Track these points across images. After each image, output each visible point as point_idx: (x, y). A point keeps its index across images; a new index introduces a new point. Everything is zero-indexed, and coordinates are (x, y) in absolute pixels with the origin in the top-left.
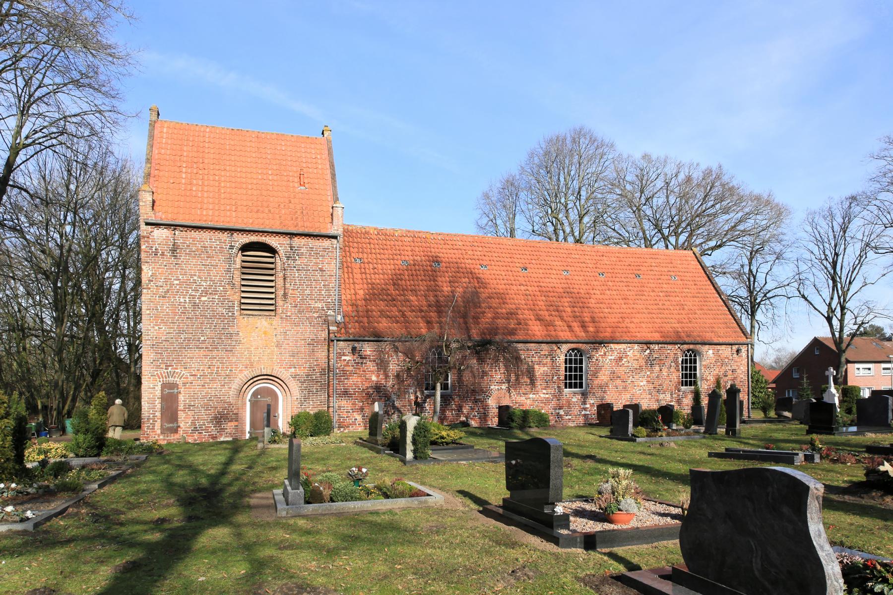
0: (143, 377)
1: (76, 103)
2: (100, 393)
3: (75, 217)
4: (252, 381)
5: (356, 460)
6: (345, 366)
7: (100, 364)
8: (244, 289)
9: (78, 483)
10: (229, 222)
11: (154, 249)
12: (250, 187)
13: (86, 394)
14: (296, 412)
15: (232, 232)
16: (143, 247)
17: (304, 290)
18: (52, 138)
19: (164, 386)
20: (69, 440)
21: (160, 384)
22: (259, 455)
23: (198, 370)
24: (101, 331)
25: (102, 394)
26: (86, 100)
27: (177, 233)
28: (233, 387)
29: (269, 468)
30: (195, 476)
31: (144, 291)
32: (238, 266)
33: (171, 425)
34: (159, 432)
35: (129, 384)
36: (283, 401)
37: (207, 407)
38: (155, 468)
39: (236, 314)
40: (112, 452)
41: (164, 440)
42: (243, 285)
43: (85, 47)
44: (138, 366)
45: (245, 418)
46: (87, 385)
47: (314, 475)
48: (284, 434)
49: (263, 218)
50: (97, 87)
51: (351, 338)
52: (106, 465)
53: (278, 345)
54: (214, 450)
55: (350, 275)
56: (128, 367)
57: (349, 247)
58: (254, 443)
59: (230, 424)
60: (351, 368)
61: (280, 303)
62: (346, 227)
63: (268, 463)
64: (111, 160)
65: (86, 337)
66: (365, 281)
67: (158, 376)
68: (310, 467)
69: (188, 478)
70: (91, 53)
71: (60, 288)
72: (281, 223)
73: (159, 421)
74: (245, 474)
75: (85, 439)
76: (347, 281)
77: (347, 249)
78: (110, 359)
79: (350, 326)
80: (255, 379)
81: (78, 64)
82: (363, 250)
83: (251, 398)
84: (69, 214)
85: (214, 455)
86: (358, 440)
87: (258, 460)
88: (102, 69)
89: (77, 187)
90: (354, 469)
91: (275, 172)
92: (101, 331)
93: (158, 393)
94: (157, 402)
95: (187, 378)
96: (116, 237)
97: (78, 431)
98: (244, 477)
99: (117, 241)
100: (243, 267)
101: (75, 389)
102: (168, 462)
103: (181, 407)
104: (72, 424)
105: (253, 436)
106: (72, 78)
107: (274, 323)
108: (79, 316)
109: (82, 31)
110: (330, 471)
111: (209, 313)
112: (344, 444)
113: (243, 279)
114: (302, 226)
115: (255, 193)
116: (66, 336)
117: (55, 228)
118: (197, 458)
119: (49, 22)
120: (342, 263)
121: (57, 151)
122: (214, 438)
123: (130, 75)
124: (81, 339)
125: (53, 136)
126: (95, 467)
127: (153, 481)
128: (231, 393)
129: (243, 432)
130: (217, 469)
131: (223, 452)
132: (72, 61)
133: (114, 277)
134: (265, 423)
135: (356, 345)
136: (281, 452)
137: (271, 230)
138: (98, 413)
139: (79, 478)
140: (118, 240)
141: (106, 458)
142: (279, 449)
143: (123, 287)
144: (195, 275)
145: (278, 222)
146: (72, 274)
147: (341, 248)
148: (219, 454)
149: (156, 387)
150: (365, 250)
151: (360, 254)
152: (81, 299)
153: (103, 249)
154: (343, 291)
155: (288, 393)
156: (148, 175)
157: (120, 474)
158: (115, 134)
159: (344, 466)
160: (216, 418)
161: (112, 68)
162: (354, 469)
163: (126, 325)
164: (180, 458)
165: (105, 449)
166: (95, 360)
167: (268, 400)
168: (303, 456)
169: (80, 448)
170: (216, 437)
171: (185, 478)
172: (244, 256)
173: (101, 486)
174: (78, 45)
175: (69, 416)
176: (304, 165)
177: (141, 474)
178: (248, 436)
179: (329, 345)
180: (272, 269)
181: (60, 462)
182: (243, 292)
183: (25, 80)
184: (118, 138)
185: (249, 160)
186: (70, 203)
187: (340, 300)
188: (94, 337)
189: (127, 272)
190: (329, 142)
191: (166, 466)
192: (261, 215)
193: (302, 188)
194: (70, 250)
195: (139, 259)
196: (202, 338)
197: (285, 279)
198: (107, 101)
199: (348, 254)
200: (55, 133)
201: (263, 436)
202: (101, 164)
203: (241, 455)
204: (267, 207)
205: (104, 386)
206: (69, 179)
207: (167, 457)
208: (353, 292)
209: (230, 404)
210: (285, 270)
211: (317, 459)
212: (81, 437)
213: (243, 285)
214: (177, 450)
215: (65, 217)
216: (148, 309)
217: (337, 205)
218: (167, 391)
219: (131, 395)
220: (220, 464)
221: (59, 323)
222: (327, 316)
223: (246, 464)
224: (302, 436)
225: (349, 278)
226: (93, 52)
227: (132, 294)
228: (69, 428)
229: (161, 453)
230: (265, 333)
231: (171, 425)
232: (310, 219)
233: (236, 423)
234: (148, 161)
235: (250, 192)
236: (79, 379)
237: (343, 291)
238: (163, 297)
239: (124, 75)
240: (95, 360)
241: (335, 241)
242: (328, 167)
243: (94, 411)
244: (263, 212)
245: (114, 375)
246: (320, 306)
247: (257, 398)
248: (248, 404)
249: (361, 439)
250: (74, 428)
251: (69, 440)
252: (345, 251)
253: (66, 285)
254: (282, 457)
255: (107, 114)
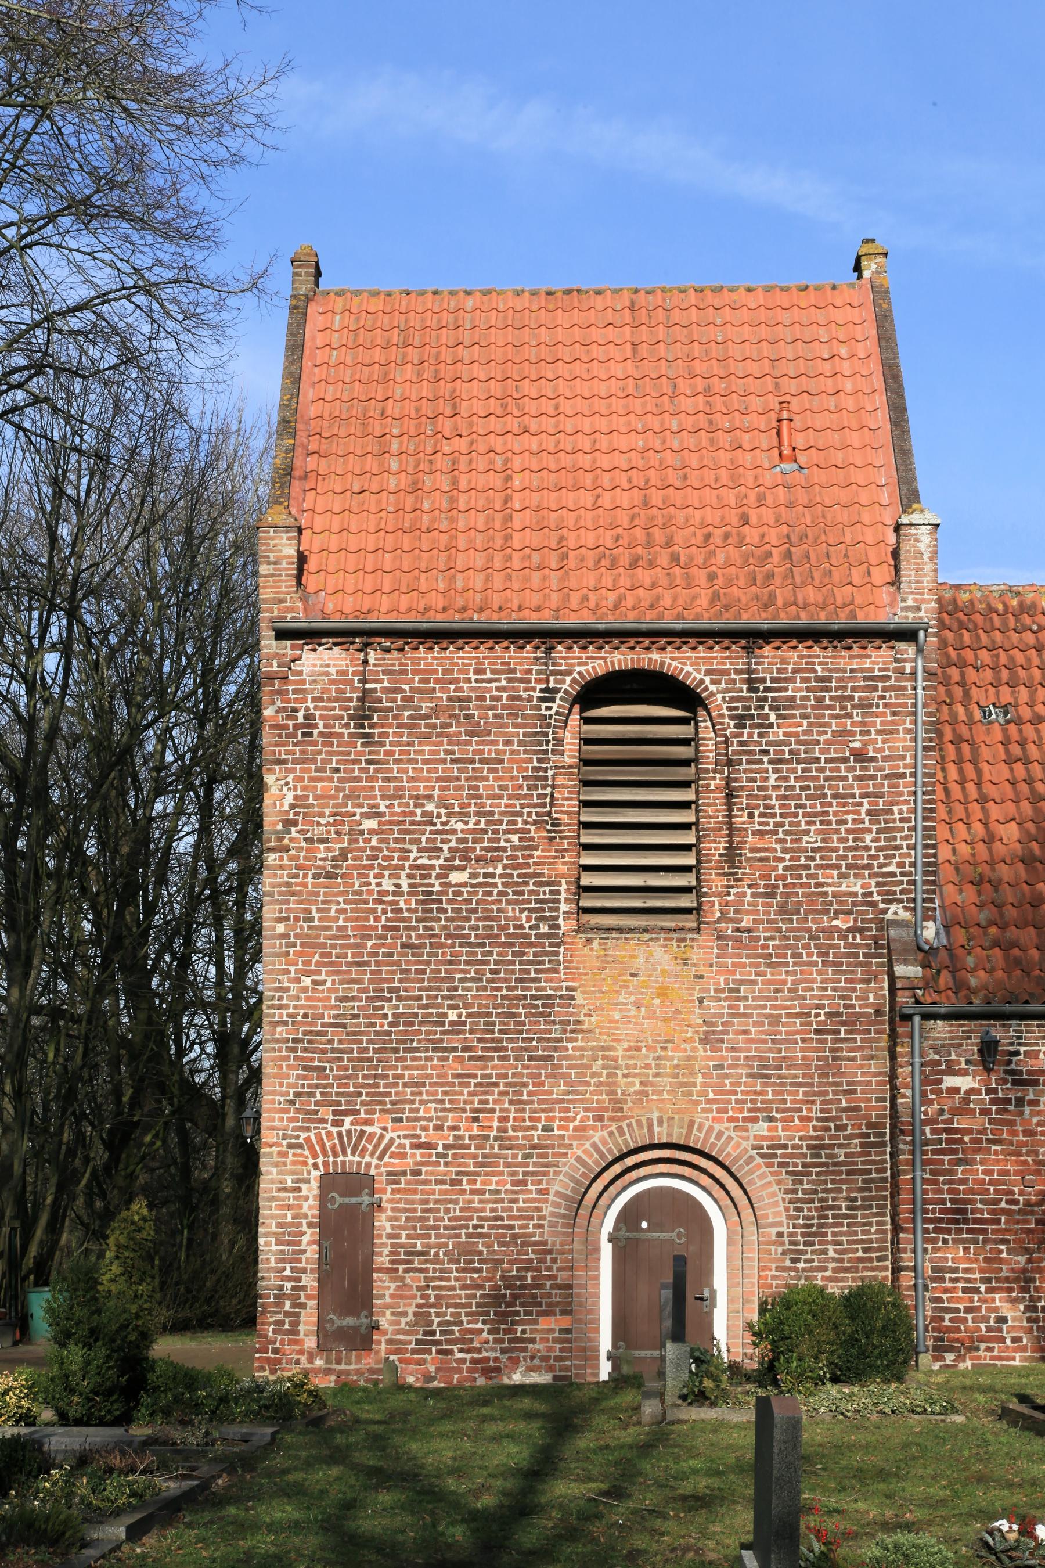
0: (264, 1150)
1: (80, 270)
2: (135, 1207)
3: (70, 626)
4: (617, 1168)
5: (1010, 1485)
6: (955, 1111)
7: (135, 1103)
8: (587, 838)
9: (69, 1517)
10: (538, 609)
11: (301, 715)
12: (606, 480)
13: (89, 1204)
14: (777, 1283)
15: (550, 642)
16: (268, 712)
17: (798, 834)
18: (11, 387)
19: (330, 1182)
20: (37, 1362)
21: (316, 1174)
22: (645, 1448)
23: (438, 1128)
24: (138, 993)
25: (139, 1208)
26: (107, 256)
27: (372, 657)
28: (556, 1187)
29: (684, 1498)
30: (432, 1513)
31: (271, 858)
32: (570, 757)
33: (350, 1321)
34: (311, 1343)
35: (217, 1173)
36: (730, 1242)
37: (465, 1256)
38: (299, 1476)
39: (565, 925)
40: (167, 1413)
41: (328, 1372)
42: (588, 825)
43: (108, 98)
44: (248, 1113)
45: (597, 1304)
46: (94, 1173)
47: (850, 1536)
48: (734, 1368)
49: (654, 586)
50: (138, 211)
51: (977, 1004)
52: (150, 1459)
53: (710, 1037)
54: (493, 1418)
55: (969, 768)
56: (217, 1111)
57: (962, 665)
58: (629, 1397)
59: (544, 1323)
60: (977, 1122)
61: (714, 882)
62: (948, 595)
63: (682, 1476)
64: (181, 434)
65: (95, 1012)
66: (1024, 788)
67: (311, 1148)
68: (832, 1502)
69: (409, 1519)
70: (125, 109)
71: (22, 855)
72: (715, 597)
73: (312, 1303)
74: (599, 1516)
75: (87, 1363)
76: (956, 790)
77: (954, 673)
78: (162, 1089)
79: (970, 961)
80: (630, 1161)
81: (89, 149)
82: (1013, 675)
83: (616, 1228)
84: (54, 618)
85: (496, 1438)
86: (1014, 1405)
87: (646, 1466)
88: (157, 155)
89: (81, 528)
90: (1004, 1524)
91: (689, 422)
92: (138, 993)
93: (310, 1207)
94: (305, 1239)
95: (403, 1155)
96: (188, 682)
97: (68, 1335)
98: (596, 1528)
99: (187, 697)
100: (587, 762)
101: (61, 1188)
102: (338, 1456)
103: (383, 1259)
104: (50, 1310)
105: (625, 1369)
106: (72, 197)
107: (695, 955)
108: (74, 943)
109: (102, 49)
110: (908, 1527)
111: (473, 928)
112: (959, 1419)
113: (587, 804)
114: (787, 605)
115: (625, 499)
116: (38, 1010)
117: (13, 666)
118: (437, 1444)
119: (12, 39)
120: (936, 727)
121: (27, 424)
122: (491, 1371)
123: (237, 160)
124: (76, 1020)
125: (17, 377)
126: (116, 1461)
127: (296, 1526)
128: (547, 1210)
129: (590, 1355)
130: (505, 1493)
131: (521, 1426)
132: (73, 142)
133: (179, 812)
134: (668, 1323)
135: (997, 1032)
136: (725, 1437)
137: (678, 626)
138: (128, 1273)
139: (70, 1495)
140: (194, 693)
141: (148, 1431)
142: (718, 1426)
143: (203, 847)
144: (430, 797)
145: (704, 601)
146: (59, 808)
147: (930, 674)
148: (510, 1436)
149: (304, 1186)
150: (1022, 673)
151: (1005, 690)
152: (84, 890)
153: (147, 727)
154: (943, 832)
155: (747, 1212)
156: (285, 474)
157: (192, 1490)
158: (190, 355)
159: (963, 1506)
160: (497, 1299)
161: (186, 147)
162: (1004, 1524)
163: (213, 970)
164: (378, 1442)
165: (145, 1399)
166: (117, 1093)
167: (676, 1236)
168: (807, 1458)
169: (72, 1391)
170: (498, 1370)
171: (397, 1522)
172: (588, 721)
173: (135, 1532)
174: (90, 94)
175: (42, 1280)
176: (793, 386)
177: (257, 1497)
178: (605, 1370)
179: (893, 1036)
180: (686, 763)
181: (16, 1440)
182: (587, 847)
183: (287, 528)
184: (196, 365)
185: (603, 389)
186: (57, 583)
187: (932, 866)
188: (116, 1014)
189: (218, 795)
190: (880, 293)
191: (335, 1471)
192: (645, 576)
193: (786, 466)
194: (54, 730)
195: (254, 747)
196: (453, 1016)
197: (729, 796)
198: (166, 252)
199: (958, 691)
200: (20, 369)
201: (661, 1375)
202: (146, 452)
203: (584, 1442)
204: (668, 544)
205: (143, 1178)
206: (56, 509)
207: (339, 1439)
208: (978, 829)
209: (544, 1250)
210: (729, 763)
211: (860, 1474)
212: (75, 1356)
213: (588, 825)
214: (369, 1412)
215: (44, 628)
216: (280, 920)
217: (915, 518)
218: (339, 1200)
219: (225, 1210)
220: (507, 1472)
221: (18, 971)
222: (884, 925)
223: (605, 1477)
224: (800, 1377)
225: (962, 782)
226: (132, 105)
227: (232, 866)
228: (41, 1324)
229: (317, 1422)
230: (663, 992)
231: (350, 1321)
232: (817, 575)
233: (565, 1322)
234: (287, 426)
235: (606, 500)
236: (71, 1153)
237: (943, 832)
238: (329, 876)
239: (217, 164)
240: (117, 1093)
241: (908, 650)
242: (878, 382)
243: (116, 1269)
244: (652, 565)
245: (174, 1139)
246: (858, 889)
247: (639, 1229)
248: (606, 1251)
249: (1023, 1399)
250: (55, 1323)
251: (37, 1362)
252: (946, 683)
253: (42, 846)
254: (731, 1458)
255: (169, 291)
